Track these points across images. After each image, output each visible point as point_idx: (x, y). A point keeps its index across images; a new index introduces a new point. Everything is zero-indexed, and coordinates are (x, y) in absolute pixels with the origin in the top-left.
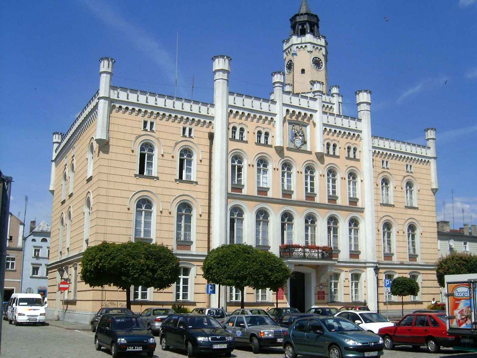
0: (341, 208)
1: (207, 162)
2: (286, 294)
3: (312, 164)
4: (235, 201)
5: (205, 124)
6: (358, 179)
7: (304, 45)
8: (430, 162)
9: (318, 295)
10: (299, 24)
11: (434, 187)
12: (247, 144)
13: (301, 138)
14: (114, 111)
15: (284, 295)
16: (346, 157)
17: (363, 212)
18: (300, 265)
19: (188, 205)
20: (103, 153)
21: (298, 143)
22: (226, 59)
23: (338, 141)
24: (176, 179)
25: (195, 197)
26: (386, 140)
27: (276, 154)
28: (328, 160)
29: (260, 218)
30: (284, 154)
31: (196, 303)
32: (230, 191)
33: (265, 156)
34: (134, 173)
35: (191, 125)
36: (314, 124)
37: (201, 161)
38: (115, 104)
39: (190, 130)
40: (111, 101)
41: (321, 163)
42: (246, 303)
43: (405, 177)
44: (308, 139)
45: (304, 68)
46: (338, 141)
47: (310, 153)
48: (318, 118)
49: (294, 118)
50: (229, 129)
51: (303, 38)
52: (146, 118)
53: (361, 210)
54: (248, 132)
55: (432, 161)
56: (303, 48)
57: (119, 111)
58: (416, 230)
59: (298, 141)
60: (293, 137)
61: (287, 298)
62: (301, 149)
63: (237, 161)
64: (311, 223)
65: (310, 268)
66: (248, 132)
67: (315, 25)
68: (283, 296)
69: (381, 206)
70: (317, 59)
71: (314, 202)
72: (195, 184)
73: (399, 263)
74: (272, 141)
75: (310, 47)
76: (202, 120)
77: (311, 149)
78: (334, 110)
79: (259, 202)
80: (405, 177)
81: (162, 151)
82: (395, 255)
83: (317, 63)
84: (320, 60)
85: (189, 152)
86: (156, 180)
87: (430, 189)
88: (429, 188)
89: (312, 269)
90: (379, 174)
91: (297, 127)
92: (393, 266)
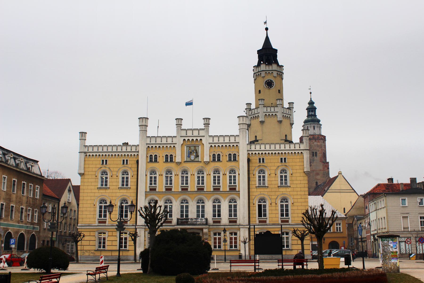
1: (136, 176)
7: (259, 73)
11: (305, 170)
21: (192, 157)
39: (127, 160)
43: (278, 166)
45: (260, 90)
53: (238, 193)
59: (193, 157)
60: (189, 155)
74: (175, 159)
75: (263, 74)
84: (272, 81)
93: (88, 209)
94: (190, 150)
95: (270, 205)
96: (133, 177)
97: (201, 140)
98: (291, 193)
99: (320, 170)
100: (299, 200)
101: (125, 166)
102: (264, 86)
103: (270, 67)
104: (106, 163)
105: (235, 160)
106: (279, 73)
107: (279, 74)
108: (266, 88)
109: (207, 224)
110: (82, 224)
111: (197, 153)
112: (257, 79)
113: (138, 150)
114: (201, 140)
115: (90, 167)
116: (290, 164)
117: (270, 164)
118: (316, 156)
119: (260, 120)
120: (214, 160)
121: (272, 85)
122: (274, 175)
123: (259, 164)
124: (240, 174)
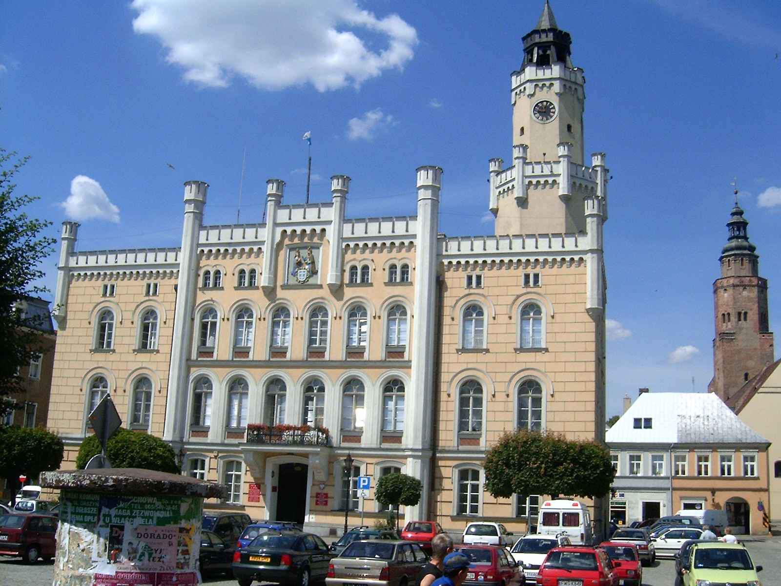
0: (295, 364)
2: (264, 495)
3: (322, 303)
5: (166, 276)
7: (522, 88)
9: (315, 499)
11: (588, 306)
12: (222, 291)
13: (307, 267)
14: (74, 281)
15: (261, 496)
16: (235, 287)
18: (289, 454)
21: (302, 274)
23: (372, 260)
24: (515, 347)
28: (349, 293)
29: (142, 389)
30: (276, 295)
32: (194, 356)
33: (246, 304)
35: (526, 269)
39: (156, 285)
40: (67, 269)
43: (518, 297)
44: (319, 266)
46: (372, 260)
47: (320, 287)
49: (296, 241)
52: (106, 282)
53: (407, 365)
54: (375, 270)
55: (588, 257)
56: (523, 92)
57: (561, 266)
59: (302, 273)
60: (295, 268)
61: (265, 500)
62: (308, 283)
63: (400, 312)
68: (259, 498)
70: (545, 103)
71: (323, 359)
75: (529, 88)
80: (518, 297)
83: (543, 111)
84: (551, 104)
87: (583, 310)
90: (457, 301)
91: (304, 253)
92: (205, 447)
94: (297, 258)
96: (167, 325)
98: (550, 367)
99: (755, 349)
100: (569, 387)
101: (151, 298)
103: (548, 72)
106: (568, 85)
107: (570, 87)
111: (313, 263)
114: (323, 230)
116: (550, 289)
117: (496, 291)
118: (745, 319)
119: (516, 196)
120: (352, 283)
121: (552, 114)
123: (467, 292)
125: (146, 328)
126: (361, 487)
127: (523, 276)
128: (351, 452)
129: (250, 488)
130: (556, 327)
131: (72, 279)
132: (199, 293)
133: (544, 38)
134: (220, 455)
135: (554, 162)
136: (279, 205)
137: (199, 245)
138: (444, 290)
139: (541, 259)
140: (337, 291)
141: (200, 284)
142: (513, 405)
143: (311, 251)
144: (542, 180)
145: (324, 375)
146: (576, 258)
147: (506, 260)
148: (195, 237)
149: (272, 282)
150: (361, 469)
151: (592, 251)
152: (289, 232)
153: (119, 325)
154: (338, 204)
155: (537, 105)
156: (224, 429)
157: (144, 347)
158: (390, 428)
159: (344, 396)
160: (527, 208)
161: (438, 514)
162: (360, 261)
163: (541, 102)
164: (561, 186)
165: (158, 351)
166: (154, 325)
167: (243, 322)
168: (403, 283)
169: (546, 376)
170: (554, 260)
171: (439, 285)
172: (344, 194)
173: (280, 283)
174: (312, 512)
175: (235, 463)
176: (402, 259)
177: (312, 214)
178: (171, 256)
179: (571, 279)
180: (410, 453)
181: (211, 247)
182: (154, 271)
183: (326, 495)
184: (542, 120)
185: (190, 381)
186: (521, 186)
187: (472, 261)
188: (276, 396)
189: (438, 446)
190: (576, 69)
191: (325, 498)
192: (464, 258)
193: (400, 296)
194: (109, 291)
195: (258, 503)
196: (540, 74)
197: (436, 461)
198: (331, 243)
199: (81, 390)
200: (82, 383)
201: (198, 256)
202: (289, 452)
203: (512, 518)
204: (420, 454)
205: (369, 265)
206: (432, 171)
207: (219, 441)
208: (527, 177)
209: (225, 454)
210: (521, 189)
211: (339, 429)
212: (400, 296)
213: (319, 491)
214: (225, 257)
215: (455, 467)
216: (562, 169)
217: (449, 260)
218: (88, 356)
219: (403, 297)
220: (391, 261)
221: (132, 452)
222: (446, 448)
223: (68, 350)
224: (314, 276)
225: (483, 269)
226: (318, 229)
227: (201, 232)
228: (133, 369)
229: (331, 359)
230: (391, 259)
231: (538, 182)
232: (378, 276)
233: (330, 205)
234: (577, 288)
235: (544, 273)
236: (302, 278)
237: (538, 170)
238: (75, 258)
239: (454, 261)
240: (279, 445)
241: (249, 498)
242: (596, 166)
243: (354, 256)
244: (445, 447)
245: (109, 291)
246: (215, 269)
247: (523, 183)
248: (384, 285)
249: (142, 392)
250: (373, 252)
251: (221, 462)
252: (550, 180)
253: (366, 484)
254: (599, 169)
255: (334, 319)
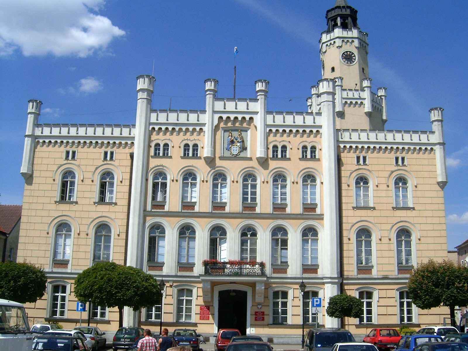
2: (213, 315)
4: (154, 218)
5: (104, 145)
6: (318, 182)
7: (332, 42)
8: (435, 150)
9: (254, 316)
10: (331, 20)
11: (440, 180)
12: (171, 159)
13: (238, 144)
15: (210, 316)
17: (323, 219)
18: (231, 283)
19: (367, 230)
20: (28, 185)
21: (235, 150)
22: (146, 78)
23: (289, 142)
25: (113, 218)
26: (362, 131)
27: (259, 165)
28: (273, 164)
31: (198, 324)
32: (149, 208)
34: (55, 200)
36: (256, 127)
37: (416, 186)
38: (39, 140)
39: (112, 153)
40: (33, 137)
41: (264, 169)
42: (164, 323)
43: (392, 172)
44: (248, 145)
45: (334, 66)
46: (289, 142)
47: (250, 159)
48: (258, 120)
49: (230, 124)
50: (268, 148)
51: (332, 34)
52: (68, 148)
53: (320, 217)
54: (291, 149)
55: (437, 148)
56: (333, 45)
58: (412, 236)
59: (235, 149)
60: (229, 145)
61: (213, 318)
62: (239, 156)
63: (161, 177)
64: (250, 236)
65: (246, 286)
66: (291, 149)
67: (348, 17)
69: (354, 209)
70: (346, 53)
72: (114, 205)
73: (381, 277)
75: (338, 42)
76: (123, 142)
77: (251, 154)
78: (365, 105)
79: (244, 219)
80: (392, 172)
81: (415, 182)
82: (375, 268)
83: (348, 57)
84: (353, 54)
85: (404, 180)
86: (97, 205)
88: (434, 181)
89: (248, 287)
90: (351, 173)
91: (236, 134)
92: (189, 279)
93: (36, 240)
94: (230, 137)
95: (379, 242)
96: (123, 184)
97: (252, 120)
98: (416, 220)
101: (108, 162)
102: (340, 60)
104: (73, 157)
105: (313, 157)
107: (363, 44)
108: (344, 63)
109: (263, 274)
110: (76, 270)
111: (243, 141)
112: (327, 51)
113: (134, 134)
114: (251, 118)
115: (43, 163)
116: (415, 168)
120: (275, 157)
121: (353, 60)
122: (385, 188)
123: (357, 167)
124: (323, 183)
125: (103, 186)
126: (315, 305)
127: (395, 158)
128: (163, 279)
129: (201, 309)
130: (419, 194)
131: (37, 145)
132: (151, 160)
133: (344, 12)
134: (175, 284)
135: (349, 90)
136: (216, 98)
137: (151, 124)
138: (341, 165)
139: (406, 147)
140: (264, 162)
141: (152, 153)
142: (394, 246)
143: (241, 133)
144: (354, 101)
145: (256, 223)
146: (429, 148)
147: (383, 147)
148: (148, 118)
149: (213, 155)
150: (67, 287)
151: (439, 144)
152: (224, 118)
153: (80, 182)
154: (263, 100)
155: (343, 53)
156: (177, 264)
157: (102, 200)
158: (184, 261)
159: (180, 238)
160: (344, 119)
161: (346, 324)
162: (280, 142)
163: (346, 52)
164: (366, 106)
165: (116, 204)
166: (72, 184)
167: (188, 183)
168: (311, 159)
169: (414, 226)
170: (415, 148)
171: (339, 162)
172: (266, 93)
173: (217, 156)
174: (252, 326)
175: (185, 291)
176: (311, 142)
177: (242, 106)
178: (125, 132)
179: (425, 162)
180: (329, 280)
181: (161, 125)
182: (111, 142)
183: (263, 313)
184: (348, 63)
185: (147, 227)
186: (341, 104)
187: (360, 146)
188: (218, 239)
189: (344, 275)
190: (365, 33)
191: (262, 315)
192: (372, 144)
193: (312, 168)
194: (71, 156)
195: (208, 321)
196: (345, 34)
197: (343, 285)
198: (259, 128)
199: (48, 233)
200: (88, 229)
201: (150, 131)
202: (230, 281)
203: (398, 324)
204: (337, 281)
205: (287, 145)
206: (332, 83)
207: (174, 274)
208: (344, 98)
209: (179, 284)
210: (341, 106)
211: (271, 264)
212: (312, 168)
213: (258, 310)
214: (172, 134)
215: (357, 290)
216: (366, 94)
217: (344, 145)
218: (54, 206)
219: (315, 169)
220: (303, 143)
221: (135, 282)
222: (350, 277)
223: (35, 201)
224: (244, 151)
225: (367, 152)
226: (247, 117)
227: (151, 114)
228: (95, 218)
229: (261, 212)
230: (303, 142)
231: (351, 103)
232: (294, 153)
233: (256, 100)
234: (431, 168)
235: (409, 157)
236: (235, 153)
237: (350, 94)
238: (40, 129)
239: (348, 146)
240: (222, 275)
241: (200, 317)
242: (381, 96)
243: (275, 139)
244: (349, 275)
245: (71, 156)
246: (164, 142)
247: (342, 102)
248: (299, 160)
249: (102, 235)
250: (289, 136)
251: (176, 290)
252: (359, 101)
253: (318, 303)
254: (383, 98)
255: (262, 183)
